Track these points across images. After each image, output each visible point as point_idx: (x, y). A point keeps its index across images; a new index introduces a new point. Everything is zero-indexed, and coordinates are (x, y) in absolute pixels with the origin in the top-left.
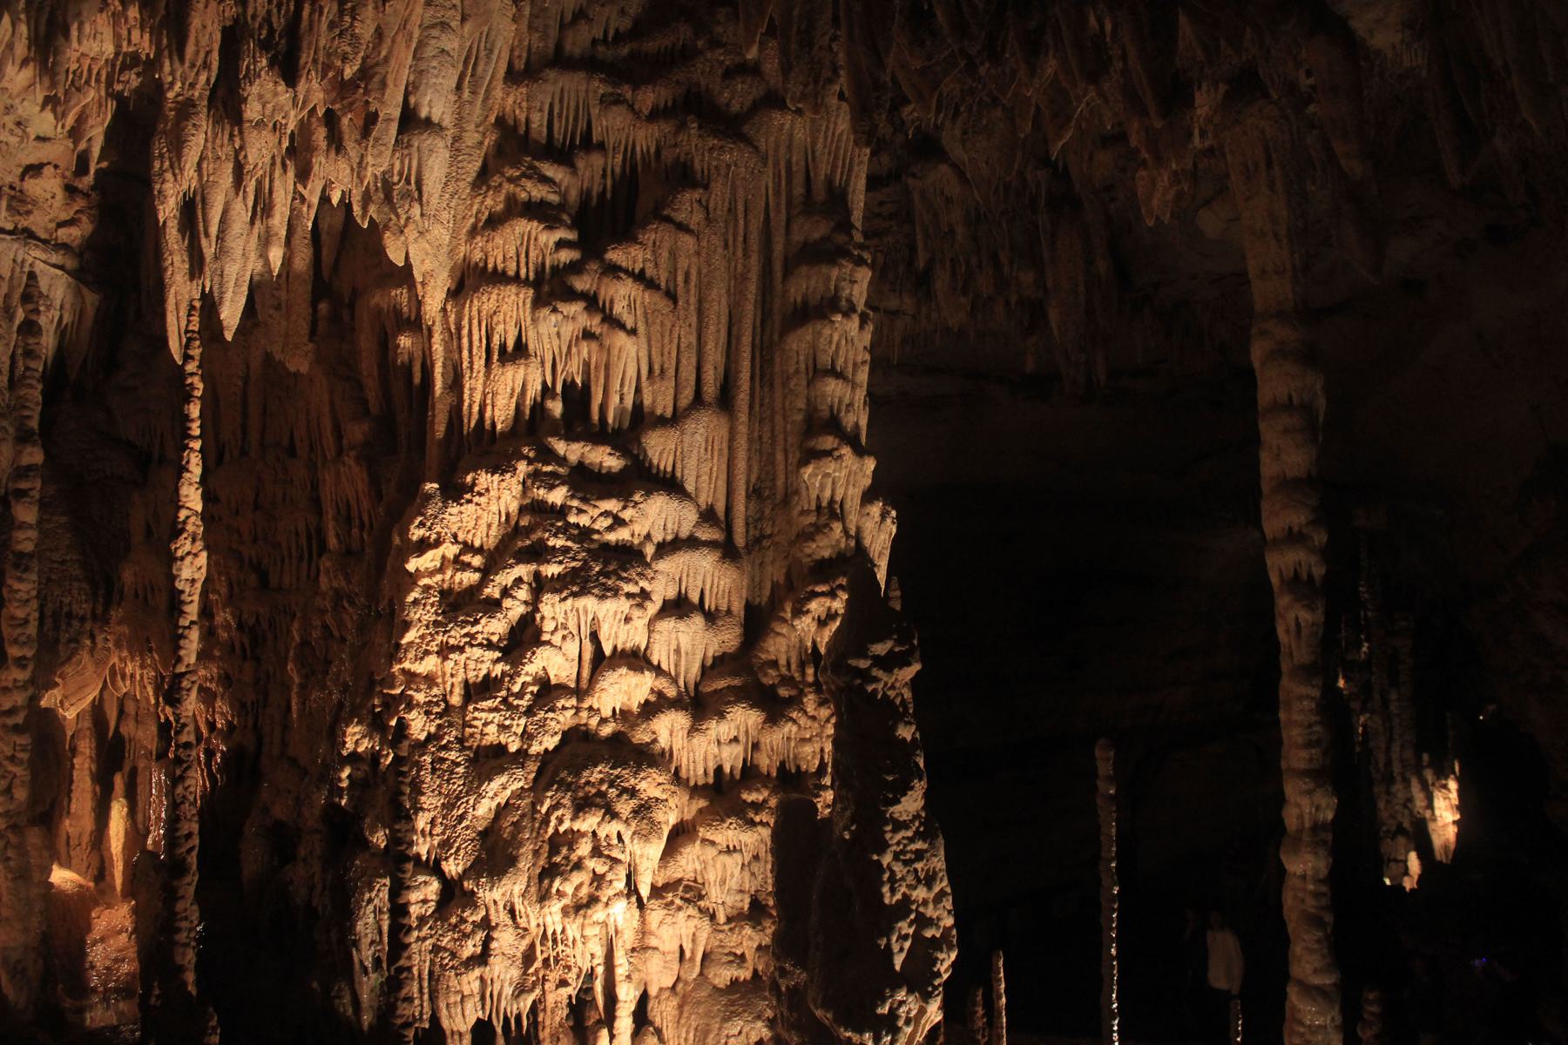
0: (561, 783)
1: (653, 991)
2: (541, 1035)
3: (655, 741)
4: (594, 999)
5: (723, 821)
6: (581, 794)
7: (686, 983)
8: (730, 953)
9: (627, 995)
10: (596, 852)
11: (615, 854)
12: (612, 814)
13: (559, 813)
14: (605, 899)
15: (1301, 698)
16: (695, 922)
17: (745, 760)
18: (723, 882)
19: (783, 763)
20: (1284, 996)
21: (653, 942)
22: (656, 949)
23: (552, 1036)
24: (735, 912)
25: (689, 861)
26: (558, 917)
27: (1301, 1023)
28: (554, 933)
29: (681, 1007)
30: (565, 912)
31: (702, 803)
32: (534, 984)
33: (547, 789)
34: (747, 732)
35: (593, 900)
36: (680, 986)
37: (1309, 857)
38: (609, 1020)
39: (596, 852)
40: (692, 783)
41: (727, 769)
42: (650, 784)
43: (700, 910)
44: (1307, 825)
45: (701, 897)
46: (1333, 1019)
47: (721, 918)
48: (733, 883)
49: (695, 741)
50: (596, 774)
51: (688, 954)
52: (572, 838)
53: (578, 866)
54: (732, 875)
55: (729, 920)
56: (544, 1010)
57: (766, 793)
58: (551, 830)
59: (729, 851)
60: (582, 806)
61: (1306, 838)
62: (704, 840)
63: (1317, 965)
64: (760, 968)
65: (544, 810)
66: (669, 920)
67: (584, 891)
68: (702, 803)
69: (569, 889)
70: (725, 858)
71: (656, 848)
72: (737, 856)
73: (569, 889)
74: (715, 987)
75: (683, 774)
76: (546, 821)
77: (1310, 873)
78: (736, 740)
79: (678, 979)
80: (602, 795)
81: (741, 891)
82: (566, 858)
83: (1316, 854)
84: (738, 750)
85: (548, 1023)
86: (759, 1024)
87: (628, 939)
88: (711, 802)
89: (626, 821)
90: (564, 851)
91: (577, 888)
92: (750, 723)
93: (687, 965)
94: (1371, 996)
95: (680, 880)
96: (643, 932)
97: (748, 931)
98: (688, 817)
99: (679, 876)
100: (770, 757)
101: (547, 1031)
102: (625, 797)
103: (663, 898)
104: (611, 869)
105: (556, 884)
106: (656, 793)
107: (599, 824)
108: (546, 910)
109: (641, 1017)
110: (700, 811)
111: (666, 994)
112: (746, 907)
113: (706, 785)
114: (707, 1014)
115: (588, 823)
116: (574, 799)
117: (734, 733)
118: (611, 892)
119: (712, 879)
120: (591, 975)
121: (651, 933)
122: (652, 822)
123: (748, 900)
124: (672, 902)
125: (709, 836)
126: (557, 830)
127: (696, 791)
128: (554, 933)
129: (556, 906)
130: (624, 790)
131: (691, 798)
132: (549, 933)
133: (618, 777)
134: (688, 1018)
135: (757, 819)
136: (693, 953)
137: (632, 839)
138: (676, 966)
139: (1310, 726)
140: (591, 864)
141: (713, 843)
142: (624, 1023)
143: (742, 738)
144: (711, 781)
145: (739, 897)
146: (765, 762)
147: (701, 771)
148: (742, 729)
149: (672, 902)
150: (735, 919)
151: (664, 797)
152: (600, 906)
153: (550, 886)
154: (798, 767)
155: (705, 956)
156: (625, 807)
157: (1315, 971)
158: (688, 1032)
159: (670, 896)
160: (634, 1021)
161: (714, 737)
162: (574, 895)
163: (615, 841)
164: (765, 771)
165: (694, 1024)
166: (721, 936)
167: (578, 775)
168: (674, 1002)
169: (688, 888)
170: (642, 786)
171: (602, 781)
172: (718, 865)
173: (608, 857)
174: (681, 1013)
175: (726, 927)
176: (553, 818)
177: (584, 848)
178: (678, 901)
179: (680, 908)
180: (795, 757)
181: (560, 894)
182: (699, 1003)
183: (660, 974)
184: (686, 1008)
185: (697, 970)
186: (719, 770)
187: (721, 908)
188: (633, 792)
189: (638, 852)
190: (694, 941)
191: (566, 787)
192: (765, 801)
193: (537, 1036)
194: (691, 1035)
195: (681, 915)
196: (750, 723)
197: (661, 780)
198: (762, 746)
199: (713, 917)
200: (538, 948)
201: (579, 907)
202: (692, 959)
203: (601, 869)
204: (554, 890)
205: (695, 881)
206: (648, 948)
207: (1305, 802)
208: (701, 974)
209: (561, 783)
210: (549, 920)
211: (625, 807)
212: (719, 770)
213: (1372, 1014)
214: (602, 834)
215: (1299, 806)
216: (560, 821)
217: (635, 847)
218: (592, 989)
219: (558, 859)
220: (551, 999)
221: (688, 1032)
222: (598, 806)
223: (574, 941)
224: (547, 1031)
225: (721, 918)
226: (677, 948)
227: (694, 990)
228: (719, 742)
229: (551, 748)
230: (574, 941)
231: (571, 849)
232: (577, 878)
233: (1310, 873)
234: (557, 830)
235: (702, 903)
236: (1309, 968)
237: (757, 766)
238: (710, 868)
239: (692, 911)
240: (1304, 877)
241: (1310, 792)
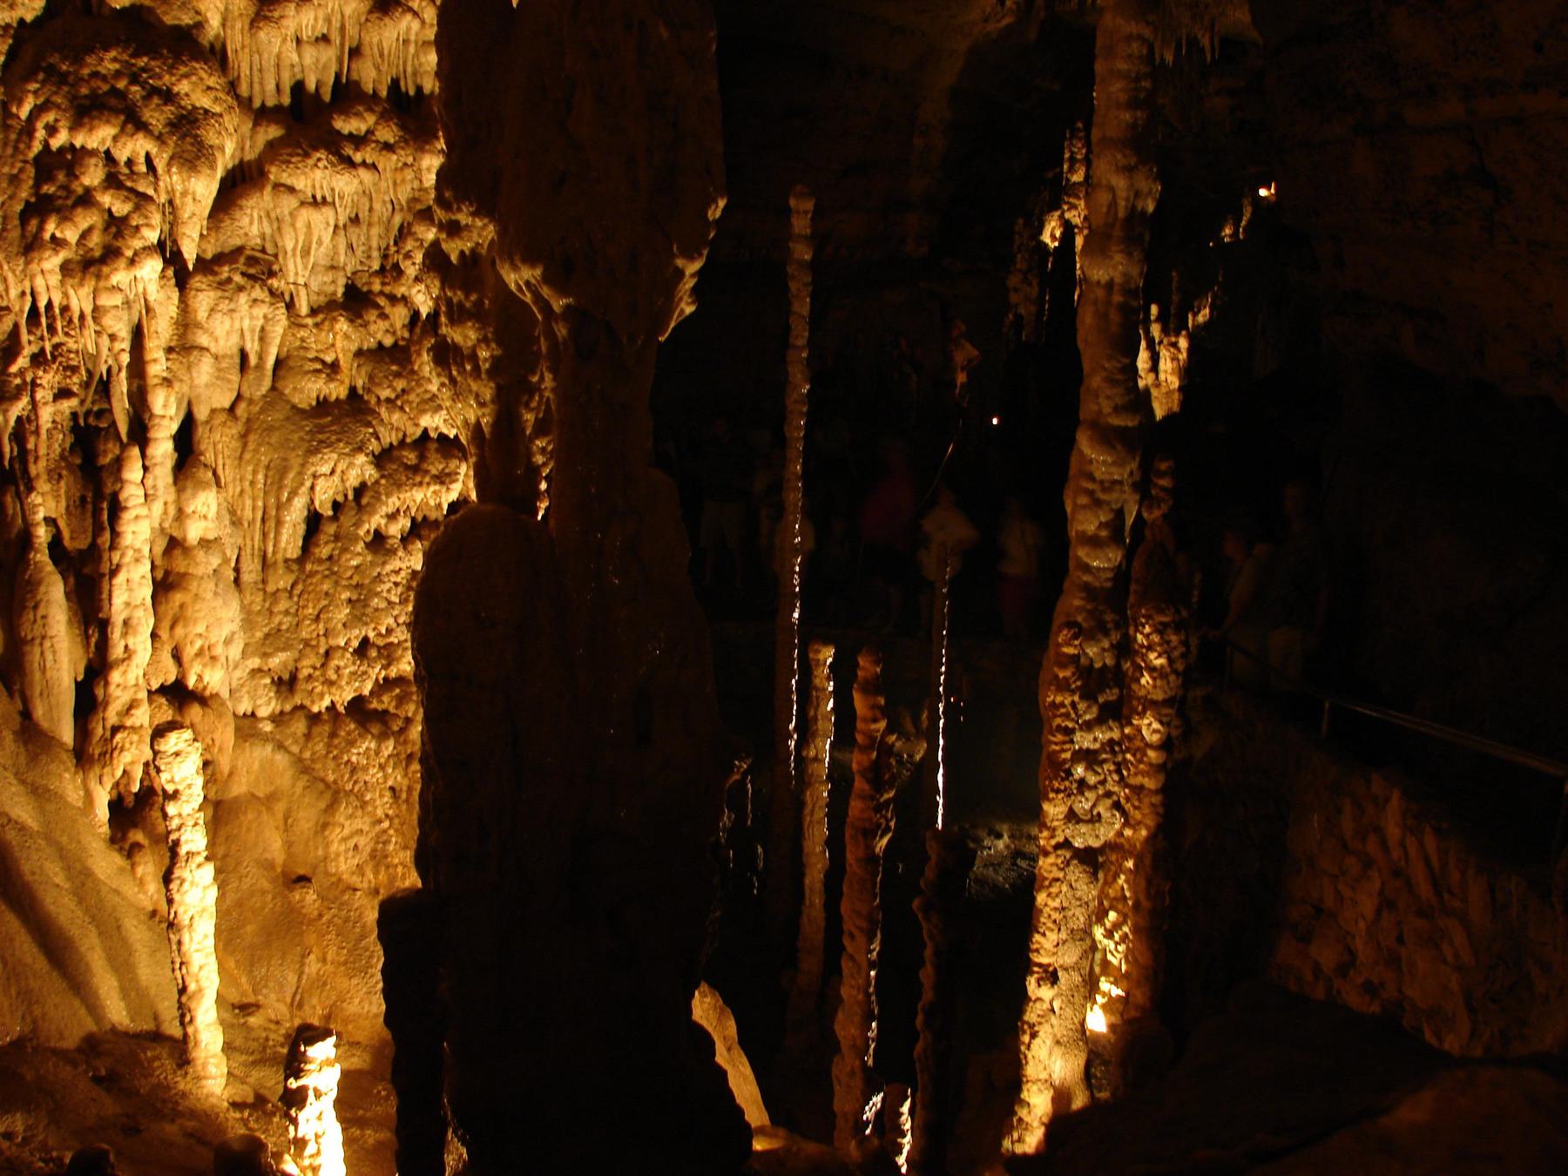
0: (51, 71)
1: (201, 414)
2: (33, 470)
3: (199, 25)
4: (114, 424)
5: (307, 155)
6: (84, 91)
7: (251, 402)
8: (317, 359)
9: (166, 410)
10: (113, 181)
11: (144, 187)
12: (134, 122)
13: (50, 117)
14: (129, 253)
15: (1129, 38)
16: (260, 311)
17: (338, 76)
18: (306, 252)
19: (395, 83)
20: (1072, 441)
21: (203, 340)
22: (203, 349)
23: (49, 472)
24: (322, 300)
25: (251, 223)
26: (55, 279)
27: (1092, 478)
28: (49, 305)
29: (244, 436)
30: (65, 269)
31: (274, 132)
32: (19, 390)
33: (30, 76)
34: (342, 28)
35: (111, 253)
36: (241, 410)
37: (1118, 257)
38: (140, 433)
39: (113, 181)
40: (257, 104)
41: (311, 86)
42: (196, 89)
43: (272, 293)
44: (1121, 214)
45: (272, 274)
46: (1131, 473)
47: (304, 309)
48: (320, 254)
49: (262, 34)
50: (109, 62)
51: (253, 360)
52: (73, 158)
53: (86, 200)
54: (320, 242)
55: (314, 312)
56: (37, 432)
57: (371, 119)
58: (37, 147)
59: (316, 203)
60: (85, 112)
61: (1117, 232)
62: (277, 186)
63: (1119, 401)
64: (360, 383)
65: (24, 113)
66: (224, 306)
67: (95, 240)
68: (274, 132)
69: (71, 234)
70: (306, 214)
71: (205, 188)
72: (328, 212)
73: (71, 234)
74: (294, 407)
75: (244, 90)
76: (28, 130)
77: (1118, 280)
78: (325, 39)
79: (239, 397)
80: (122, 95)
81: (333, 268)
82: (65, 187)
83: (1130, 254)
84: (329, 55)
85: (42, 451)
86: (361, 459)
87: (161, 332)
88: (289, 129)
89: (160, 139)
90: (61, 177)
91: (85, 235)
92: (348, 11)
93: (251, 376)
94: (1163, 466)
95: (240, 250)
96: (185, 322)
97: (342, 325)
98: (250, 155)
99: (238, 242)
100: (378, 69)
101: (42, 463)
102: (156, 100)
103: (215, 274)
104: (137, 208)
105: (51, 227)
106: (204, 101)
107: (115, 139)
108: (34, 267)
109: (185, 440)
110: (271, 145)
111: (222, 417)
112: (340, 291)
113: (278, 108)
114: (284, 445)
115: (100, 136)
116: (73, 98)
117: (322, 29)
118: (137, 244)
119: (289, 245)
120: (105, 388)
121: (198, 325)
122: (200, 144)
123: (342, 281)
124: (229, 280)
125: (285, 178)
126: (46, 145)
127: (262, 115)
128: (49, 305)
129: (52, 262)
130: (155, 91)
131: (256, 124)
132: (42, 304)
133: (144, 70)
134: (256, 451)
135: (358, 158)
136: (261, 357)
137: (169, 165)
138: (235, 377)
139: (1138, 79)
140: (106, 199)
141: (291, 190)
142: (163, 448)
143: (335, 37)
144: (286, 100)
145: (328, 278)
146: (370, 76)
147: (271, 86)
148: (336, 24)
149: (229, 280)
150: (325, 310)
151: (217, 109)
152: (122, 263)
153: (41, 228)
154: (419, 89)
155: (279, 363)
156: (156, 117)
157: (1117, 410)
158: (255, 472)
159: (225, 272)
160: (176, 449)
161: (291, 32)
162: (79, 243)
163: (143, 169)
164: (369, 88)
165: (264, 460)
166: (303, 333)
167: (78, 61)
168: (235, 429)
169: (252, 261)
170: (183, 87)
171: (118, 74)
172: (300, 224)
173: (132, 190)
174: (245, 445)
175: (310, 321)
176: (40, 125)
177: (92, 176)
178: (238, 278)
179: (241, 289)
180: (415, 74)
181: (57, 243)
182: (270, 429)
183: (210, 387)
184: (252, 437)
185: (267, 383)
186: (298, 87)
187: (303, 292)
188: (169, 96)
189: (179, 188)
190: (262, 339)
191: (57, 78)
192: (370, 132)
193: (26, 471)
194: (260, 477)
195: (243, 298)
196: (348, 11)
197: (212, 82)
198: (366, 50)
199: (290, 306)
200: (25, 337)
201: (90, 265)
202: (260, 366)
203: (121, 208)
204: (47, 236)
205: (263, 251)
206: (193, 347)
207: (1120, 183)
208: (273, 388)
209: (51, 71)
210: (40, 282)
211: (156, 117)
212: (298, 87)
213: (1163, 489)
214: (122, 155)
215: (1112, 189)
216: (52, 130)
217: (173, 180)
218: (110, 411)
219: (49, 189)
220: (46, 415)
221: (255, 472)
222: (117, 112)
223: (82, 316)
224: (42, 463)
225: (304, 309)
226: (235, 351)
227: (262, 411)
228: (299, 41)
229: (29, 18)
230: (82, 316)
231: (73, 175)
232: (87, 219)
233: (1118, 280)
234: (46, 145)
235: (274, 282)
236: (1107, 407)
237: (357, 84)
238: (287, 230)
239: (258, 293)
240: (1110, 285)
241: (1129, 170)
